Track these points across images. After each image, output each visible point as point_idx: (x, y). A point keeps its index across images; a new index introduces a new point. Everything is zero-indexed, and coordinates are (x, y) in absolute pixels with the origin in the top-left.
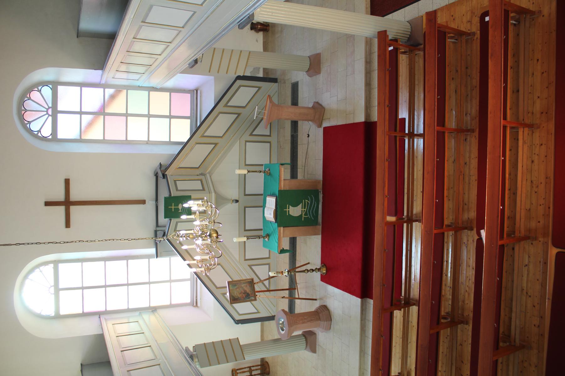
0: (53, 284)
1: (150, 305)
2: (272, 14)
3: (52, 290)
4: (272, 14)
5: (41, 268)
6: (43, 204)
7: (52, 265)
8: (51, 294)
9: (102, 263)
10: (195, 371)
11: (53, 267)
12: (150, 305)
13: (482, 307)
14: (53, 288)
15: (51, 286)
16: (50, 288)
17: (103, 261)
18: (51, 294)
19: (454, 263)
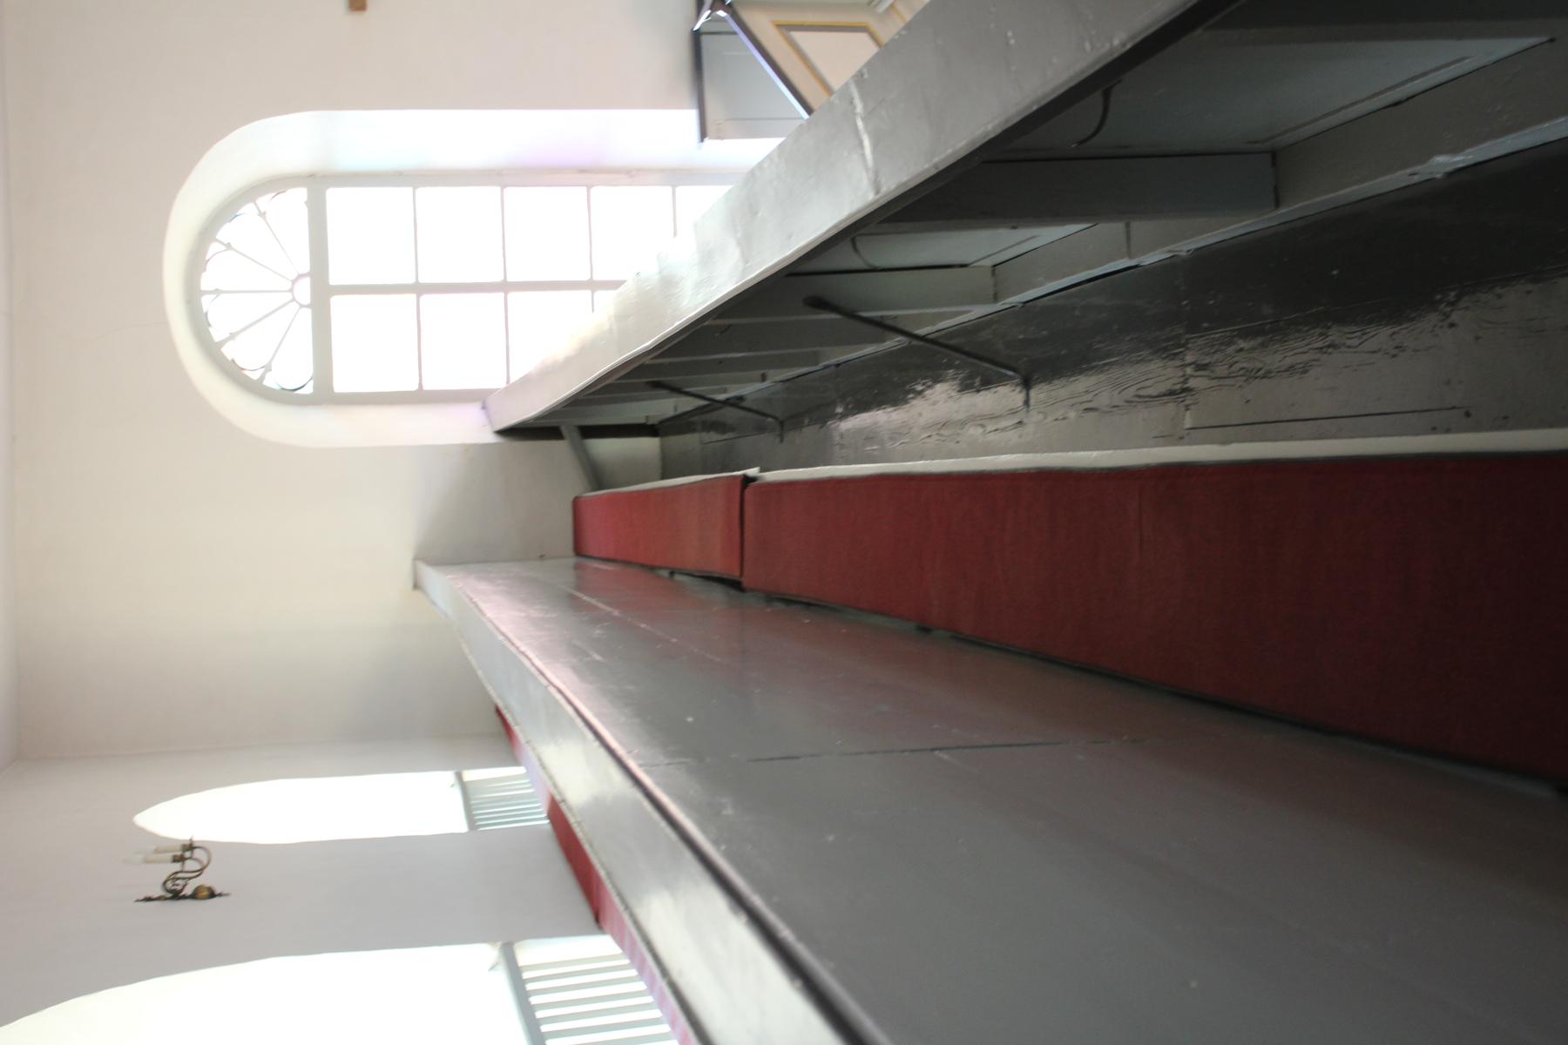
0: (305, 267)
1: (420, 385)
2: (546, 687)
3: (304, 291)
4: (546, 687)
5: (264, 201)
6: (357, 17)
7: (299, 195)
8: (302, 306)
9: (491, 192)
10: (482, 806)
11: (305, 199)
12: (420, 385)
13: (977, 459)
14: (307, 282)
15: (300, 276)
16: (294, 282)
17: (495, 184)
18: (302, 306)
19: (1101, 266)
